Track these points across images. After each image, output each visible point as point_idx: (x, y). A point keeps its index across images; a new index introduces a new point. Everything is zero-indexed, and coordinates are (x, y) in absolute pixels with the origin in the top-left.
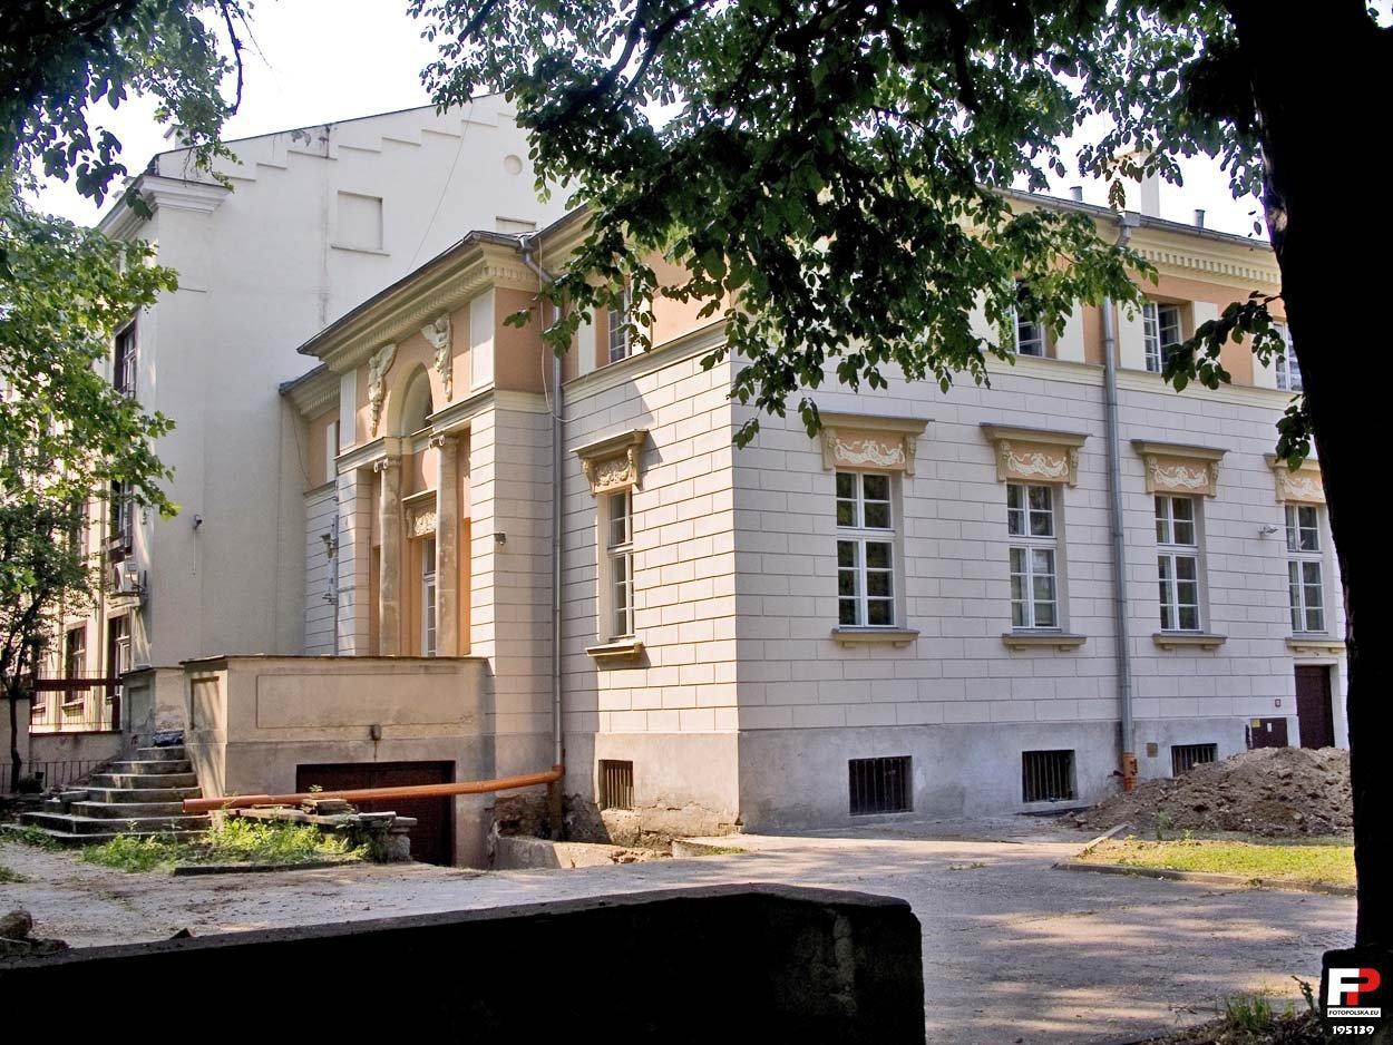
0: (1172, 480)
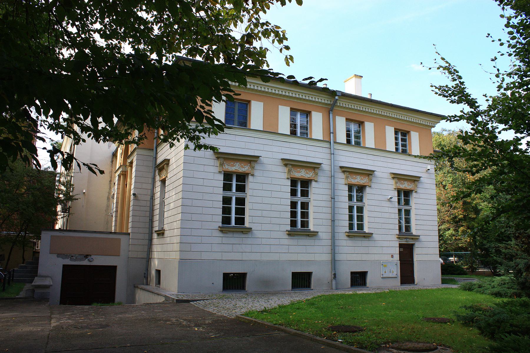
0: (299, 174)
